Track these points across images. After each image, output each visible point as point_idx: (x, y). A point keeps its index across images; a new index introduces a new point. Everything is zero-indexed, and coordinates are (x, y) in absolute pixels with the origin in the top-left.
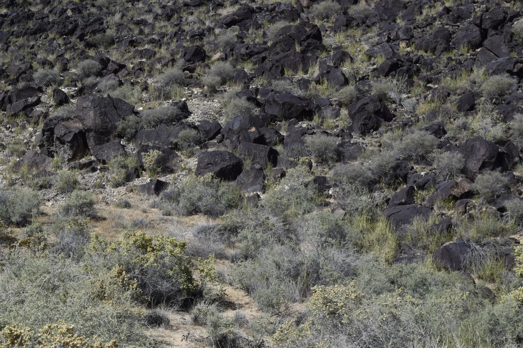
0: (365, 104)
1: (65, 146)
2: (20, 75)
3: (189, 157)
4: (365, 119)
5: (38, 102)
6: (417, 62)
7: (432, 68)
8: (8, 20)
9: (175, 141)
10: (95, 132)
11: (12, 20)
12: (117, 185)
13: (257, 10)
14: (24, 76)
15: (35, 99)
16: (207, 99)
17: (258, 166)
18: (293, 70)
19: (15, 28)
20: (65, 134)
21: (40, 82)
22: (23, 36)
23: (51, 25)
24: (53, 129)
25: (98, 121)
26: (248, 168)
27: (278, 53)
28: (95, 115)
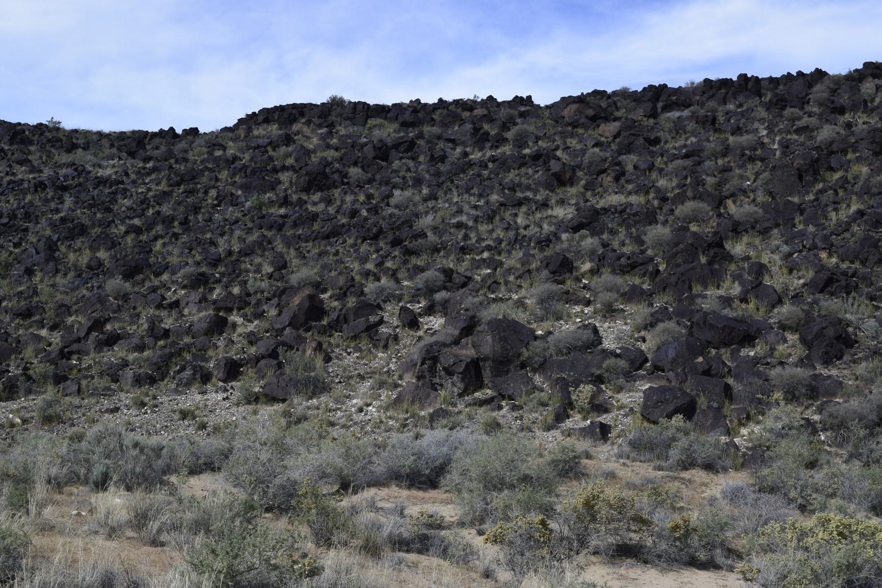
0: (823, 328)
1: (455, 378)
2: (348, 289)
3: (619, 392)
4: (827, 346)
5: (381, 322)
6: (853, 276)
7: (872, 284)
8: (289, 221)
9: (598, 372)
10: (493, 361)
11: (295, 222)
12: (548, 429)
13: (603, 212)
14: (352, 289)
15: (377, 319)
16: (608, 320)
17: (715, 405)
18: (702, 285)
19: (300, 232)
20: (454, 364)
21: (378, 297)
22: (313, 241)
23: (347, 227)
24: (437, 357)
25: (498, 348)
26: (704, 407)
27: (678, 265)
28: (493, 341)
